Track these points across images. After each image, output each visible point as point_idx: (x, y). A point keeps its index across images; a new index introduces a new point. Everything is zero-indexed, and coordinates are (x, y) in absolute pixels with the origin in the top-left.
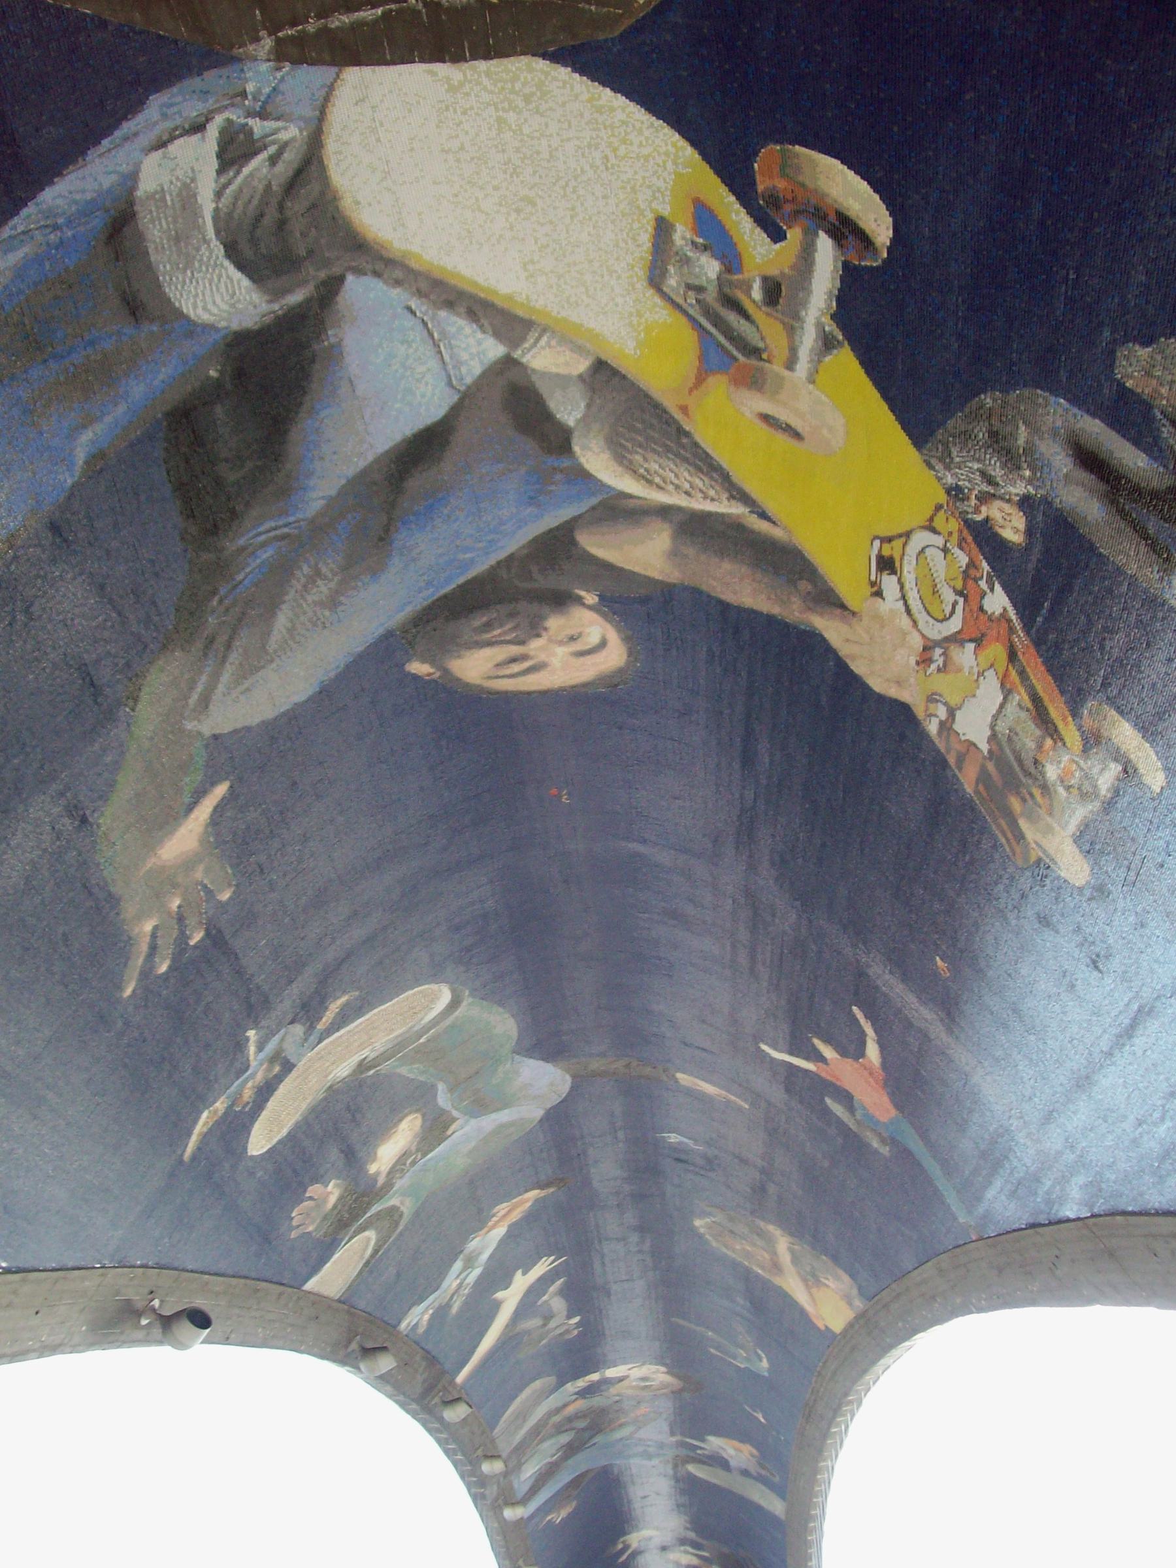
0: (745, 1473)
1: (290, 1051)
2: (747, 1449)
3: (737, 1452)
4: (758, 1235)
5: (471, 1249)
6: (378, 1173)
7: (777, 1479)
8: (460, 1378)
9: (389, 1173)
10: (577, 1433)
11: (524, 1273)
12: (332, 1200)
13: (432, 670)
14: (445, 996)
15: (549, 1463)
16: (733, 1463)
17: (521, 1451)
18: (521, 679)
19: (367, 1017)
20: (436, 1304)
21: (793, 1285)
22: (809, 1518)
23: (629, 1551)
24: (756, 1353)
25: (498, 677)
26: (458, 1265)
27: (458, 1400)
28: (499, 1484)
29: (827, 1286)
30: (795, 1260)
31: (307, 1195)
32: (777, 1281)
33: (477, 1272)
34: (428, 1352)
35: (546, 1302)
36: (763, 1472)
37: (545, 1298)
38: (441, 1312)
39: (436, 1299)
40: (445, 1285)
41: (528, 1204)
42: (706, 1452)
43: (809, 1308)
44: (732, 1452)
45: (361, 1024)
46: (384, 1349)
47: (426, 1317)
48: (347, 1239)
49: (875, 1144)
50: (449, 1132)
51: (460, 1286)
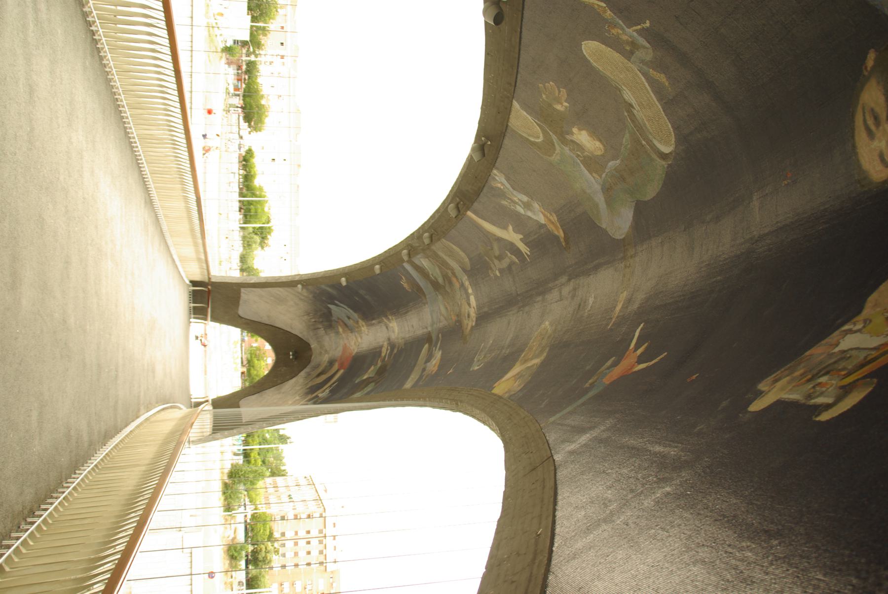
0: (424, 370)
1: (639, 54)
2: (436, 368)
4: (541, 350)
5: (533, 205)
6: (572, 134)
7: (421, 383)
9: (572, 141)
10: (443, 286)
11: (521, 239)
12: (559, 107)
13: (869, 69)
14: (666, 149)
15: (429, 273)
16: (428, 364)
17: (435, 257)
18: (863, 128)
19: (657, 103)
20: (506, 190)
21: (517, 369)
22: (402, 399)
23: (388, 323)
24: (482, 363)
25: (864, 113)
26: (525, 199)
27: (459, 211)
28: (419, 246)
29: (515, 383)
30: (529, 368)
31: (561, 89)
32: (518, 364)
33: (521, 210)
34: (482, 189)
35: (507, 255)
36: (424, 378)
37: (509, 254)
38: (502, 194)
39: (508, 189)
40: (515, 193)
41: (556, 233)
42: (434, 351)
43: (504, 379)
44: (434, 362)
45: (652, 99)
46: (484, 155)
47: (499, 185)
48: (539, 123)
49: (590, 381)
50: (594, 175)
51: (515, 203)
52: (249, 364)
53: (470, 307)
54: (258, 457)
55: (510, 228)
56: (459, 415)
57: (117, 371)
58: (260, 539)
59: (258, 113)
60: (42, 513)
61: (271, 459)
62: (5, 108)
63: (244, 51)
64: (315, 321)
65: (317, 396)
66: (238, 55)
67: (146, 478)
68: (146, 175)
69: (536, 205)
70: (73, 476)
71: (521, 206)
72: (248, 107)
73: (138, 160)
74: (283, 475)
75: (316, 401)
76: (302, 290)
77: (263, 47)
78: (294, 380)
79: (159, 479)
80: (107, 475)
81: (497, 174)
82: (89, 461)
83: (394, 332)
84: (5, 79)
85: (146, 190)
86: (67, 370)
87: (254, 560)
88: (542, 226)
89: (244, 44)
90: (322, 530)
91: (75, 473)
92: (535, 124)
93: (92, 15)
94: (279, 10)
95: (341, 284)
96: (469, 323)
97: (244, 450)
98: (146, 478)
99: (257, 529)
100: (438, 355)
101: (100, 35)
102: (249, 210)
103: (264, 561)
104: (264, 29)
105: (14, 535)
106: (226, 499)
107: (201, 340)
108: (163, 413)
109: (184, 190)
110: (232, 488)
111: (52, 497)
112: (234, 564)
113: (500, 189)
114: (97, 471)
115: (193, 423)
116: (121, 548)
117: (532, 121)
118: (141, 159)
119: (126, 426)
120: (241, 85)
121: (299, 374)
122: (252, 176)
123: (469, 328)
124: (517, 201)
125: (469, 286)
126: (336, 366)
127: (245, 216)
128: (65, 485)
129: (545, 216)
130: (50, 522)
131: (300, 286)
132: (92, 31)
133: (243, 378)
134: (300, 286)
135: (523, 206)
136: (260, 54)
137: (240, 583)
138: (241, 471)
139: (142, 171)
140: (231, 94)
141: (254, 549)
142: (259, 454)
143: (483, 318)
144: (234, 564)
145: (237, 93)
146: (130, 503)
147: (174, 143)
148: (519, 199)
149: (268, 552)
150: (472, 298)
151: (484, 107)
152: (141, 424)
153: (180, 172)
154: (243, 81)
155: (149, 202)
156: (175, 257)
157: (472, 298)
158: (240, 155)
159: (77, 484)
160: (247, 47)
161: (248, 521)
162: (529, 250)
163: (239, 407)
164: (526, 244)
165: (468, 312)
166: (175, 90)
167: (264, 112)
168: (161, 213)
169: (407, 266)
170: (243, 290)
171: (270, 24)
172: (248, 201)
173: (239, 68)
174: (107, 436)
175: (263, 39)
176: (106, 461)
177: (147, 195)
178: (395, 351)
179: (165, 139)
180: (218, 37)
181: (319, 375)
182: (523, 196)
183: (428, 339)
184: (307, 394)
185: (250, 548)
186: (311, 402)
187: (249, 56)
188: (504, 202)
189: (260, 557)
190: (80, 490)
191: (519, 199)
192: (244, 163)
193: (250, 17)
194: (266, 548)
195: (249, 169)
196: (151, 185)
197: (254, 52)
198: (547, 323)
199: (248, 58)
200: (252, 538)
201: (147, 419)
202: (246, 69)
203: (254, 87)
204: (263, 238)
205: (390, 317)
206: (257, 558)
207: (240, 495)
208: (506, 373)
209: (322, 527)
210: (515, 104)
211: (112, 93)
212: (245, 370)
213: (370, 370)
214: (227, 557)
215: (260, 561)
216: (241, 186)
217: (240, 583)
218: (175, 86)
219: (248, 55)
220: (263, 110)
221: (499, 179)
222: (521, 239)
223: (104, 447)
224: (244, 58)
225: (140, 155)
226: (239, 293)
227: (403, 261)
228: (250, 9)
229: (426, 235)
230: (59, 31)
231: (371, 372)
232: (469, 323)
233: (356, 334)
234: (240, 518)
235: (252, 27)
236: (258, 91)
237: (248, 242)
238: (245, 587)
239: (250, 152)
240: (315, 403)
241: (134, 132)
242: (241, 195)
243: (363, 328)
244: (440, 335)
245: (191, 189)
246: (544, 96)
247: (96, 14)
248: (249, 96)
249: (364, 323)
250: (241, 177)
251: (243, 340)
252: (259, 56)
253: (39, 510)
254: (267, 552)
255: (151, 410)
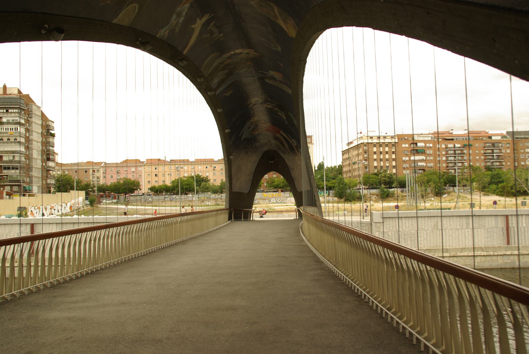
0: (281, 82)
2: (280, 74)
3: (277, 75)
8: (185, 53)
11: (200, 19)
16: (277, 79)
26: (174, 16)
27: (183, 59)
29: (289, 23)
33: (181, 20)
37: (209, 28)
43: (287, 30)
47: (166, 33)
52: (276, 188)
53: (242, 53)
54: (331, 182)
55: (193, 26)
56: (309, 59)
57: (281, 257)
58: (378, 181)
59: (128, 185)
60: (359, 291)
61: (331, 175)
62: (134, 316)
63: (92, 194)
64: (252, 148)
65: (296, 146)
66: (94, 197)
67: (342, 238)
68: (168, 245)
69: (179, 9)
70: (340, 277)
71: (179, 20)
72: (125, 191)
73: (159, 249)
74: (342, 167)
75: (299, 146)
76: (232, 156)
77: (89, 182)
78: (286, 160)
79: (343, 231)
80: (339, 254)
81: (159, 34)
82: (332, 269)
83: (258, 100)
84: (117, 316)
85: (176, 244)
86: (281, 282)
87: (389, 183)
88: (191, 6)
89: (87, 194)
90: (374, 145)
91: (338, 276)
92: (127, 8)
93: (77, 274)
94: (66, 174)
95: (229, 132)
96: (252, 53)
97: (326, 190)
98: (342, 238)
99: (372, 182)
100: (271, 73)
101: (88, 270)
102: (186, 188)
103: (390, 178)
104: (78, 183)
105: (371, 304)
106: (354, 200)
107: (263, 214)
108: (305, 233)
109: (176, 223)
110: (348, 197)
111: (351, 287)
112: (391, 195)
113: (168, 32)
114: (337, 265)
115: (311, 215)
116: (381, 248)
117: (125, 10)
118: (159, 247)
119: (312, 252)
120: (112, 195)
121: (283, 157)
122: (166, 187)
123: (255, 53)
124: (176, 22)
125: (230, 53)
126: (278, 135)
127: (190, 191)
128: (345, 281)
129: (185, 4)
130: (364, 287)
131: (231, 157)
132: (86, 274)
133: (284, 191)
134: (231, 157)
135: (179, 18)
136: (93, 185)
137: (402, 192)
138: (339, 191)
139: (166, 247)
140: (118, 201)
141: (383, 184)
142: (329, 181)
143: (249, 44)
144: (391, 195)
145: (117, 197)
146: (356, 246)
147: (148, 229)
148: (175, 20)
149: (385, 176)
150: (237, 51)
151: (118, 42)
152: (311, 244)
153: (165, 225)
154: (110, 194)
155: (183, 242)
156: (215, 228)
157: (237, 51)
158: (154, 195)
159: (344, 275)
160: (89, 192)
161: (367, 187)
162: (206, 15)
163: (302, 192)
164: (203, 17)
165: (245, 54)
166: (117, 228)
167: (127, 181)
168: (189, 236)
169: (218, 92)
170: (233, 191)
171: (74, 179)
172: (181, 189)
173: (102, 196)
174: (318, 261)
175: (84, 183)
176: (332, 261)
177: (180, 244)
178: (269, 99)
179: (146, 234)
180: (84, 209)
181: (284, 146)
182: (173, 17)
183: (262, 79)
184: (294, 153)
185: (383, 186)
186: (299, 150)
187: (95, 191)
188: (177, 30)
189: (388, 180)
190: (348, 274)
191: (175, 20)
192: (158, 192)
193: (71, 191)
194: (383, 177)
195: (162, 189)
196: (174, 241)
197: (91, 188)
198: (252, 3)
199: (96, 191)
200: (377, 185)
201: (309, 241)
202: (102, 192)
203: (113, 188)
204: (203, 180)
205: (249, 103)
206: (388, 182)
207: (352, 192)
208: (283, 29)
209: (372, 145)
210: (115, 21)
211: (121, 263)
212: (280, 190)
213: (280, 115)
214: (387, 199)
215: (390, 180)
216: (172, 194)
217: (402, 192)
218: (115, 228)
219: (94, 192)
220: (126, 182)
221: (163, 33)
222: (200, 19)
223: (324, 262)
224: (96, 194)
225: (157, 248)
226: (236, 193)
227: (215, 94)
228: (66, 191)
229: (198, 80)
230: (89, 290)
231: (282, 114)
232: (252, 53)
233: (259, 123)
234: (365, 192)
235: (76, 190)
236: (115, 185)
237: (205, 189)
238: (405, 189)
239: (152, 189)
240: (300, 148)
241: (143, 251)
242: (177, 194)
243: (256, 119)
244: (260, 72)
245: (174, 219)
246: (108, 2)
247: (76, 272)
248: (119, 191)
249: (253, 119)
250: (167, 194)
251: (263, 191)
252: (94, 185)
253: (358, 293)
254: (385, 176)
255: (303, 239)
